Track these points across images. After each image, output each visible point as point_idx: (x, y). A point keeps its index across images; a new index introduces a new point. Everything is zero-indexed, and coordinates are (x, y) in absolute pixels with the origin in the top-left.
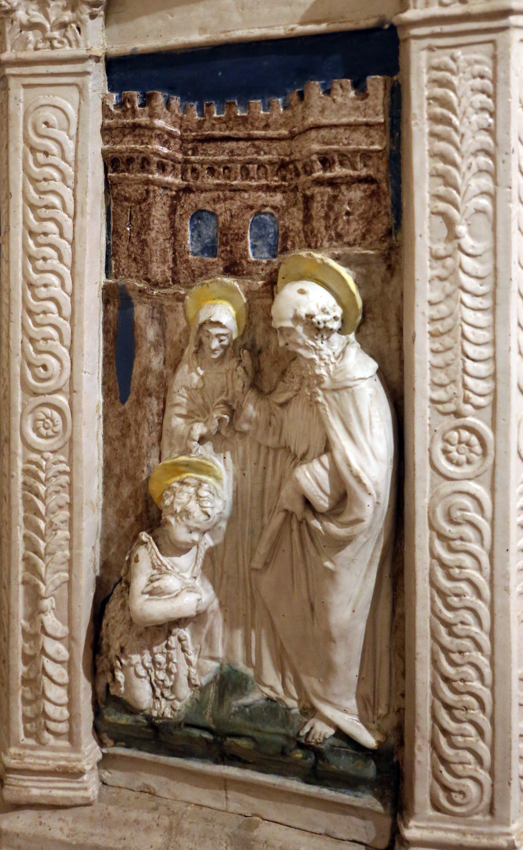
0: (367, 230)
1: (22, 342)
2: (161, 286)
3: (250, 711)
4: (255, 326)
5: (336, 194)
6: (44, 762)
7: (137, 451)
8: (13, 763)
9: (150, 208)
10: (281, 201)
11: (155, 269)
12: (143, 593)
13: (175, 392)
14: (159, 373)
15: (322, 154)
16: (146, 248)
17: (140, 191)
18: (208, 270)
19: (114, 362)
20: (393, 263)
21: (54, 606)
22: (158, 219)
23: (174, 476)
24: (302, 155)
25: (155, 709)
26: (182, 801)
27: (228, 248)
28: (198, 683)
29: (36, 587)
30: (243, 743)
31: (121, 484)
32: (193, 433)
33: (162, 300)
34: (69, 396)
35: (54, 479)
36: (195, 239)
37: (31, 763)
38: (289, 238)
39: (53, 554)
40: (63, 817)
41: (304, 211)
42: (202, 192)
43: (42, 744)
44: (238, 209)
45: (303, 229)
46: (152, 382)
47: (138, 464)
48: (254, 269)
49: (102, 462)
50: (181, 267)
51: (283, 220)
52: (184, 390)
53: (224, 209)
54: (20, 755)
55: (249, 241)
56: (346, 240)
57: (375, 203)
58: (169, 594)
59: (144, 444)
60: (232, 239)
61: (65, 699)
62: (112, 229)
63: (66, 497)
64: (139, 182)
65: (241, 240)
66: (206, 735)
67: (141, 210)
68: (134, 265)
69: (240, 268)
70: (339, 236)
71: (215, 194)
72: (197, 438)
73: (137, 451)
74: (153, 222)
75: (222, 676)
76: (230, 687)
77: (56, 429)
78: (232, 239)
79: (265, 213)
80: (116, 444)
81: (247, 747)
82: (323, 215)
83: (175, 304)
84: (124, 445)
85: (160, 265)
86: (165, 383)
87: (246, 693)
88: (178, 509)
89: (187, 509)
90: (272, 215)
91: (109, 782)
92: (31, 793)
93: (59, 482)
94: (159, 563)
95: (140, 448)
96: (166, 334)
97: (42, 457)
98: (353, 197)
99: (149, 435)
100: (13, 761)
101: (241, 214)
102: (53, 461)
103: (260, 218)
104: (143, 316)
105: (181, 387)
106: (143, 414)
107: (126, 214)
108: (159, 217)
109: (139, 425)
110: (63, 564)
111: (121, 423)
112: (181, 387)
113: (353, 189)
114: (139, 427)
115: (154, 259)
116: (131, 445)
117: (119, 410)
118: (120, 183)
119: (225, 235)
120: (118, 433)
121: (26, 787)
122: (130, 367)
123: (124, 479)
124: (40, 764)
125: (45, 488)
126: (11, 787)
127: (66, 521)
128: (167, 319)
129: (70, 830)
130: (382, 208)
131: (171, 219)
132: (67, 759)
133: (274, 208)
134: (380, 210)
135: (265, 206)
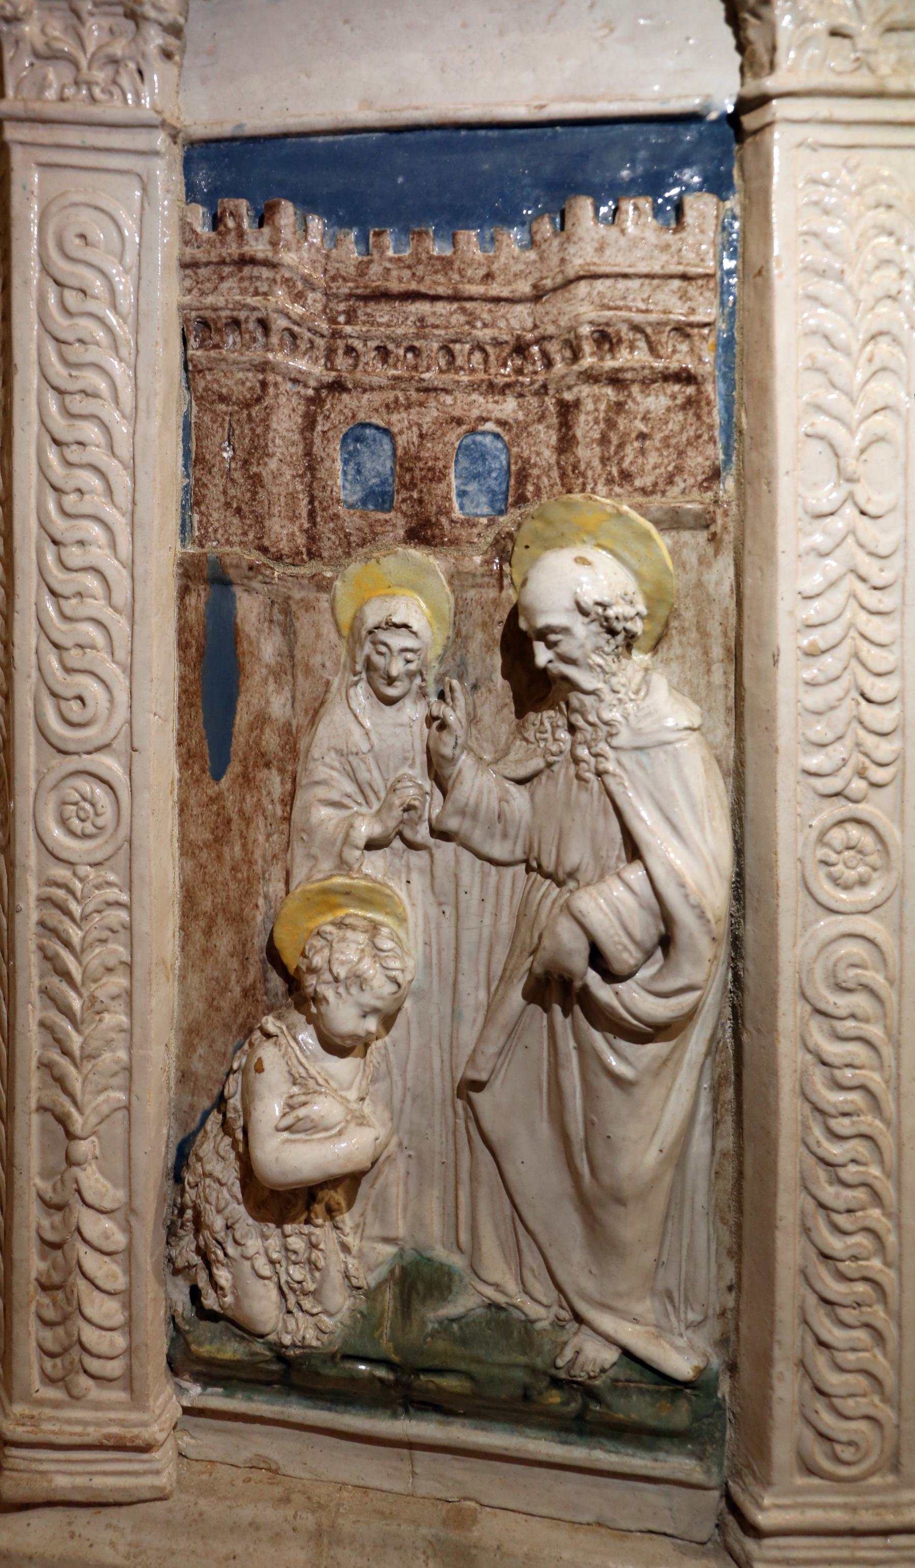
0: (676, 467)
1: (37, 652)
2: (287, 561)
3: (461, 1328)
4: (467, 638)
5: (622, 399)
6: (78, 1429)
7: (244, 868)
8: (19, 1432)
9: (268, 414)
10: (514, 411)
11: (277, 528)
12: (278, 1130)
13: (315, 760)
14: (284, 724)
15: (599, 325)
16: (259, 489)
17: (248, 384)
18: (376, 534)
19: (199, 702)
20: (719, 530)
21: (97, 1152)
22: (283, 438)
23: (322, 913)
24: (559, 326)
25: (287, 1333)
26: (330, 1482)
27: (415, 495)
28: (362, 1283)
29: (63, 1120)
30: (450, 1383)
31: (214, 930)
32: (354, 834)
33: (289, 588)
34: (124, 760)
35: (97, 917)
36: (350, 477)
37: (54, 1432)
38: (530, 480)
39: (94, 1058)
40: (114, 1522)
41: (560, 430)
42: (365, 391)
43: (75, 1398)
44: (434, 424)
45: (558, 463)
46: (271, 741)
47: (248, 893)
48: (464, 533)
49: (178, 889)
50: (325, 528)
51: (518, 445)
52: (333, 754)
53: (406, 422)
54: (32, 1417)
55: (454, 483)
56: (638, 483)
57: (691, 418)
58: (326, 1129)
59: (258, 855)
60: (422, 479)
61: (119, 1318)
62: (193, 456)
63: (122, 952)
64: (248, 365)
65: (440, 480)
66: (381, 1373)
67: (250, 418)
68: (236, 521)
69: (437, 531)
70: (626, 476)
71: (390, 396)
72: (362, 843)
73: (244, 868)
74: (273, 441)
75: (403, 1269)
76: (420, 1287)
77: (100, 822)
78: (422, 479)
79: (483, 433)
80: (204, 855)
81: (459, 1390)
82: (597, 436)
83: (312, 595)
84: (219, 857)
85: (286, 522)
86: (295, 744)
87: (450, 1297)
88: (342, 972)
89: (358, 973)
90: (497, 436)
91: (191, 1453)
92: (53, 1484)
93: (106, 921)
94: (304, 1074)
95: (251, 863)
96: (296, 652)
97: (75, 874)
98: (652, 407)
99: (267, 840)
100: (20, 1429)
101: (439, 433)
102: (95, 882)
103: (474, 442)
104: (253, 617)
105: (329, 750)
106: (255, 799)
107: (222, 426)
108: (285, 433)
109: (248, 821)
110: (114, 1074)
111: (214, 818)
112: (329, 750)
113: (653, 392)
114: (248, 824)
115: (275, 510)
116: (232, 858)
117: (209, 792)
118: (210, 369)
119: (410, 470)
120: (208, 836)
121: (43, 1473)
122: (230, 710)
123: (220, 920)
124: (71, 1434)
125: (80, 934)
126: (15, 1474)
127: (119, 996)
128: (297, 625)
129: (130, 1545)
130: (704, 428)
131: (305, 439)
132: (121, 1423)
133: (501, 423)
134: (700, 432)
135: (485, 420)
